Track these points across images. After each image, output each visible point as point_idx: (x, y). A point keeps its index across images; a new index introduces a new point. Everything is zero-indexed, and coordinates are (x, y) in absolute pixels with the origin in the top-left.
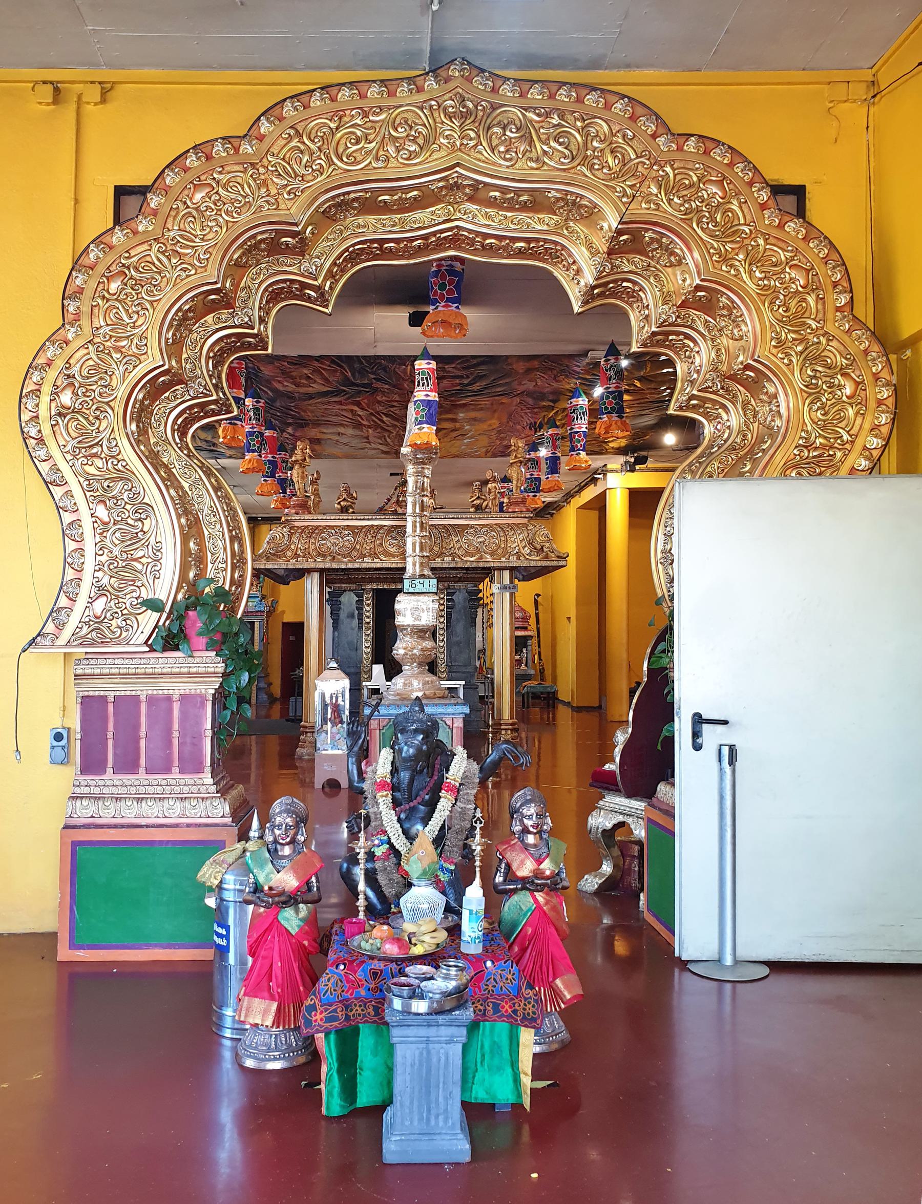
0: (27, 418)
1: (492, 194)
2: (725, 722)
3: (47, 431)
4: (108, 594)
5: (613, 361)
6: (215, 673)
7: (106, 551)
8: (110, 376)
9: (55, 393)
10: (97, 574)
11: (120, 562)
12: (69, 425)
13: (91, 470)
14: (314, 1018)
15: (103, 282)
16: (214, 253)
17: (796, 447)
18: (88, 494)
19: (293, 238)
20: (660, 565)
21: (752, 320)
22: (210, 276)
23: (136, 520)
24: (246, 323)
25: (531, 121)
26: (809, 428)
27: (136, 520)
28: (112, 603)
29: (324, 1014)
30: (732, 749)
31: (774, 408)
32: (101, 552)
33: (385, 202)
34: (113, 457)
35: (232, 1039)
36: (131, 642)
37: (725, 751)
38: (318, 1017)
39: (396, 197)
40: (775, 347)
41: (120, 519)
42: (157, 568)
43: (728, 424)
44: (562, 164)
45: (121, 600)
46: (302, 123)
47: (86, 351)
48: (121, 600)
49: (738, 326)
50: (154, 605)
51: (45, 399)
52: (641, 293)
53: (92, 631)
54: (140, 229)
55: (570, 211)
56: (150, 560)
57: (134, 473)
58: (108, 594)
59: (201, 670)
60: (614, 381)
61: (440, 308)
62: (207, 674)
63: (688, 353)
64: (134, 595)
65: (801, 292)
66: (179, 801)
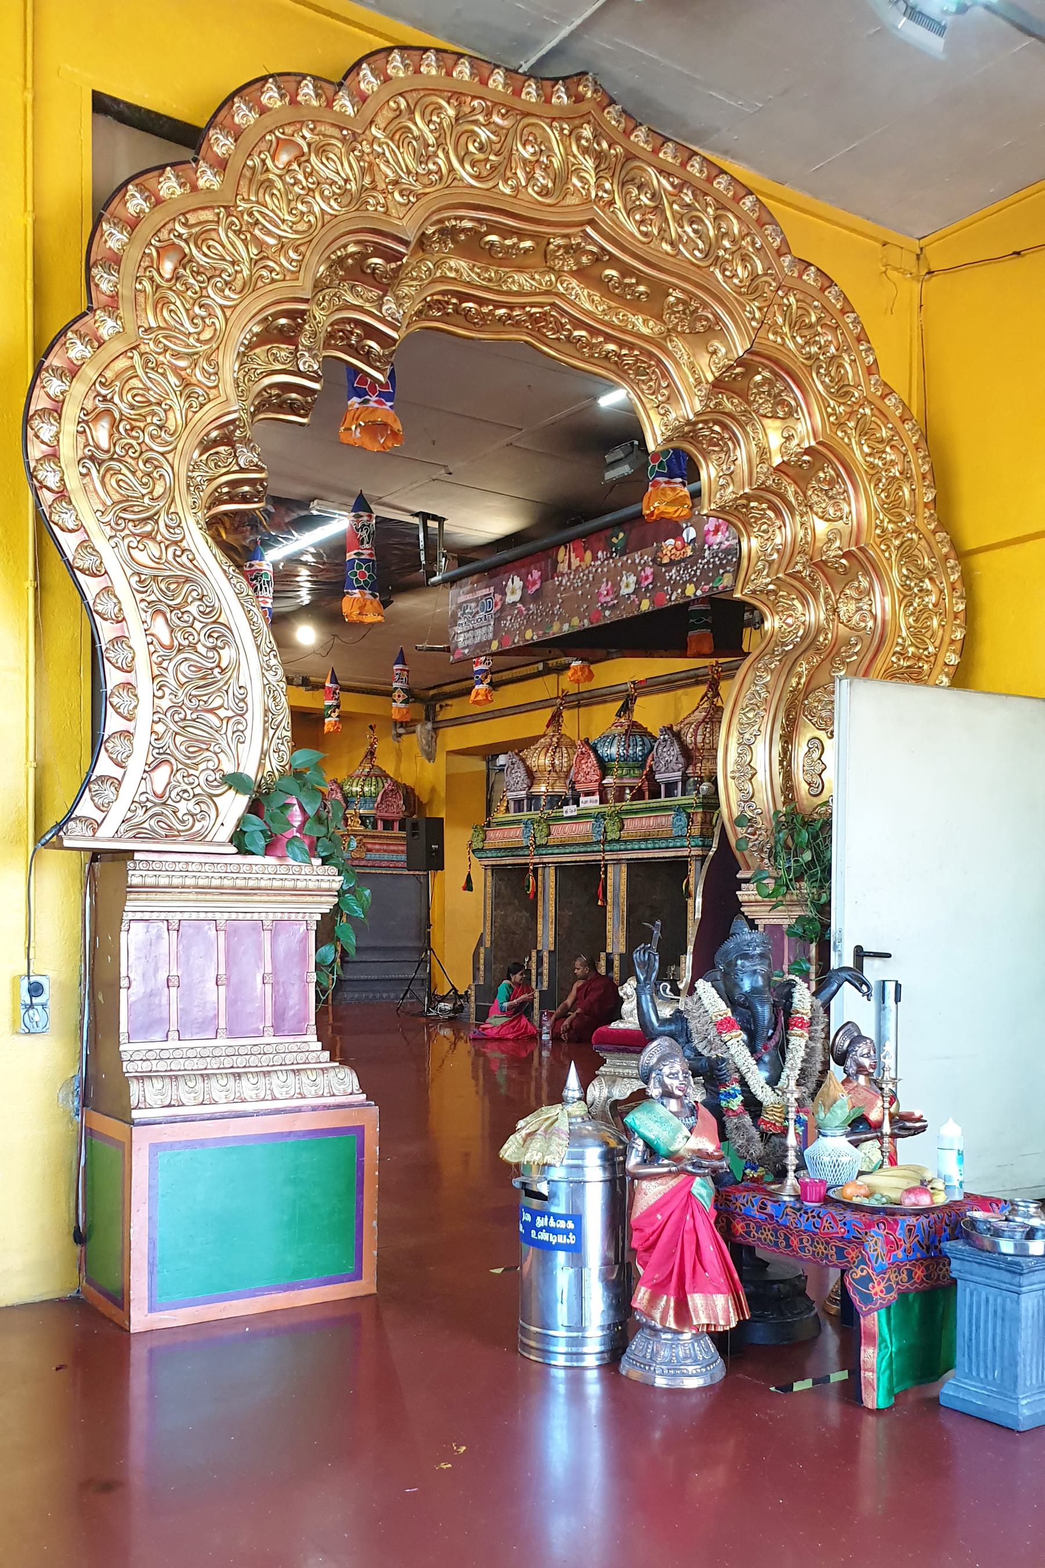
0: (38, 455)
1: (608, 272)
2: (889, 956)
3: (73, 483)
4: (173, 761)
5: (365, 518)
6: (329, 890)
7: (167, 691)
8: (165, 411)
9: (87, 422)
10: (156, 727)
11: (189, 712)
12: (107, 480)
13: (142, 557)
14: (873, 1292)
15: (150, 255)
16: (308, 254)
17: (894, 654)
18: (139, 596)
19: (388, 261)
20: (730, 780)
21: (857, 500)
22: (302, 288)
23: (209, 649)
24: (315, 372)
25: (665, 190)
26: (904, 634)
27: (209, 649)
28: (179, 776)
29: (882, 1284)
30: (898, 987)
31: (865, 607)
32: (159, 694)
33: (492, 244)
34: (176, 543)
35: (566, 1367)
36: (208, 839)
37: (890, 988)
38: (878, 1289)
39: (508, 242)
40: (879, 536)
41: (186, 643)
42: (240, 727)
43: (803, 619)
44: (695, 256)
45: (191, 771)
46: (415, 94)
47: (128, 363)
48: (191, 771)
49: (836, 504)
50: (235, 782)
51: (69, 427)
52: (730, 443)
53: (151, 817)
54: (201, 183)
55: (682, 320)
56: (230, 714)
57: (204, 574)
58: (173, 761)
59: (311, 885)
60: (367, 546)
61: (372, 404)
62: (320, 892)
63: (765, 527)
64: (211, 765)
65: (898, 479)
66: (292, 1075)
